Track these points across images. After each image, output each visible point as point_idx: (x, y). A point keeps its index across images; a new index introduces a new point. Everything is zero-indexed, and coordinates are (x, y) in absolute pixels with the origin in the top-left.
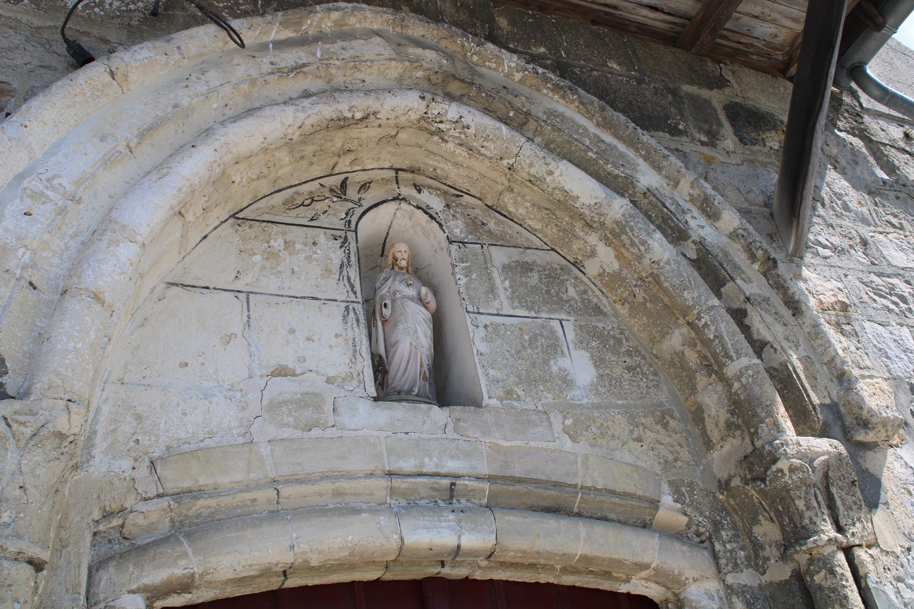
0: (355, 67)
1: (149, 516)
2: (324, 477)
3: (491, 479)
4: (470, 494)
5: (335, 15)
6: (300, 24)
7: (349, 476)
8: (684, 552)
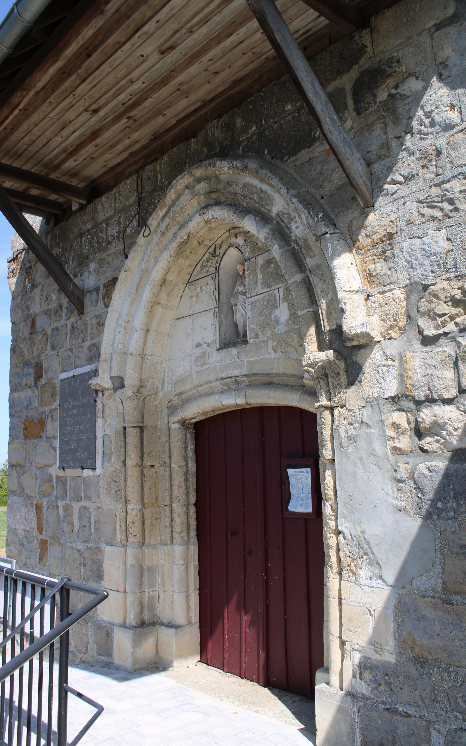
0: (182, 212)
1: (175, 401)
2: (207, 383)
3: (247, 376)
4: (243, 382)
5: (172, 191)
6: (165, 204)
7: (211, 382)
8: (307, 400)
